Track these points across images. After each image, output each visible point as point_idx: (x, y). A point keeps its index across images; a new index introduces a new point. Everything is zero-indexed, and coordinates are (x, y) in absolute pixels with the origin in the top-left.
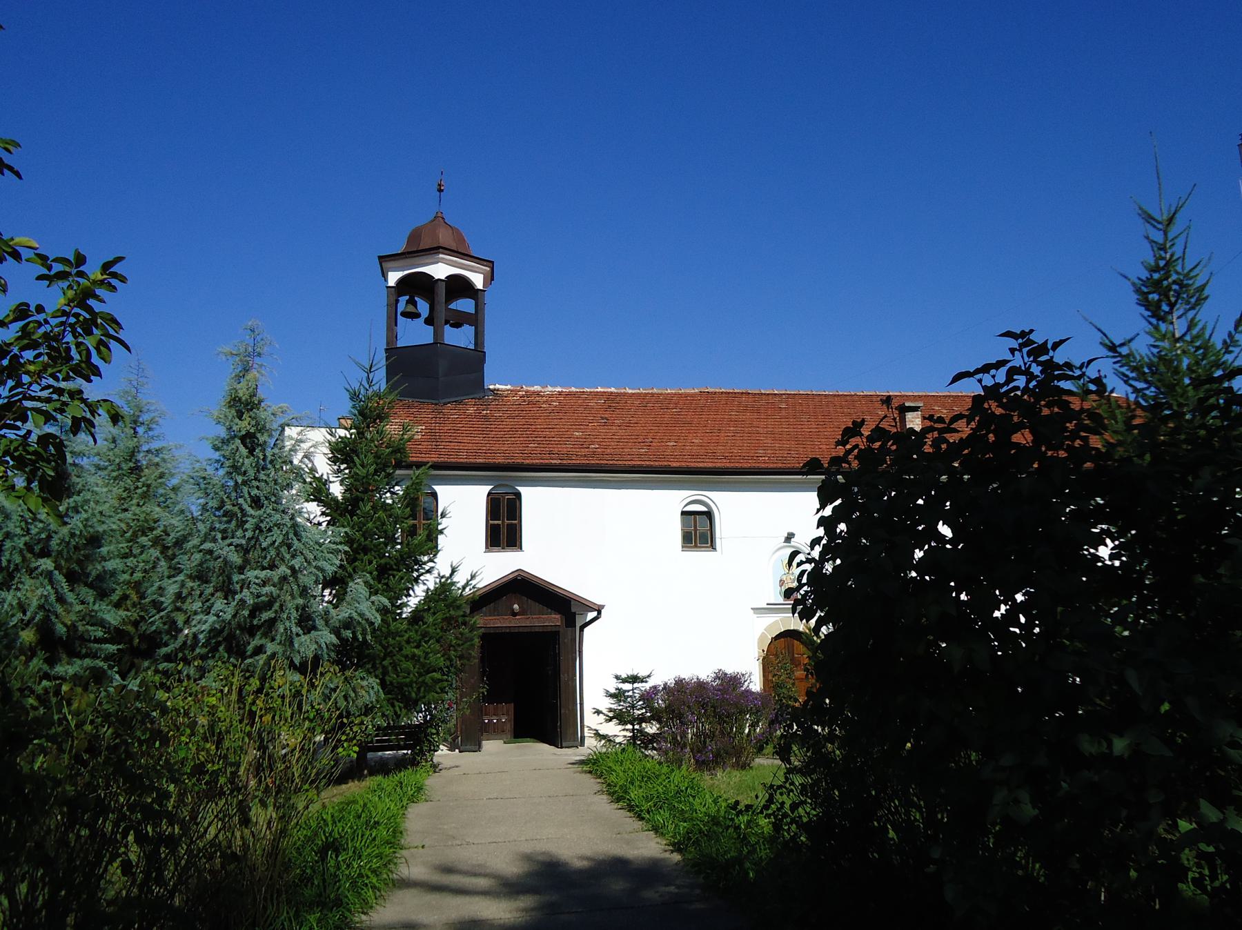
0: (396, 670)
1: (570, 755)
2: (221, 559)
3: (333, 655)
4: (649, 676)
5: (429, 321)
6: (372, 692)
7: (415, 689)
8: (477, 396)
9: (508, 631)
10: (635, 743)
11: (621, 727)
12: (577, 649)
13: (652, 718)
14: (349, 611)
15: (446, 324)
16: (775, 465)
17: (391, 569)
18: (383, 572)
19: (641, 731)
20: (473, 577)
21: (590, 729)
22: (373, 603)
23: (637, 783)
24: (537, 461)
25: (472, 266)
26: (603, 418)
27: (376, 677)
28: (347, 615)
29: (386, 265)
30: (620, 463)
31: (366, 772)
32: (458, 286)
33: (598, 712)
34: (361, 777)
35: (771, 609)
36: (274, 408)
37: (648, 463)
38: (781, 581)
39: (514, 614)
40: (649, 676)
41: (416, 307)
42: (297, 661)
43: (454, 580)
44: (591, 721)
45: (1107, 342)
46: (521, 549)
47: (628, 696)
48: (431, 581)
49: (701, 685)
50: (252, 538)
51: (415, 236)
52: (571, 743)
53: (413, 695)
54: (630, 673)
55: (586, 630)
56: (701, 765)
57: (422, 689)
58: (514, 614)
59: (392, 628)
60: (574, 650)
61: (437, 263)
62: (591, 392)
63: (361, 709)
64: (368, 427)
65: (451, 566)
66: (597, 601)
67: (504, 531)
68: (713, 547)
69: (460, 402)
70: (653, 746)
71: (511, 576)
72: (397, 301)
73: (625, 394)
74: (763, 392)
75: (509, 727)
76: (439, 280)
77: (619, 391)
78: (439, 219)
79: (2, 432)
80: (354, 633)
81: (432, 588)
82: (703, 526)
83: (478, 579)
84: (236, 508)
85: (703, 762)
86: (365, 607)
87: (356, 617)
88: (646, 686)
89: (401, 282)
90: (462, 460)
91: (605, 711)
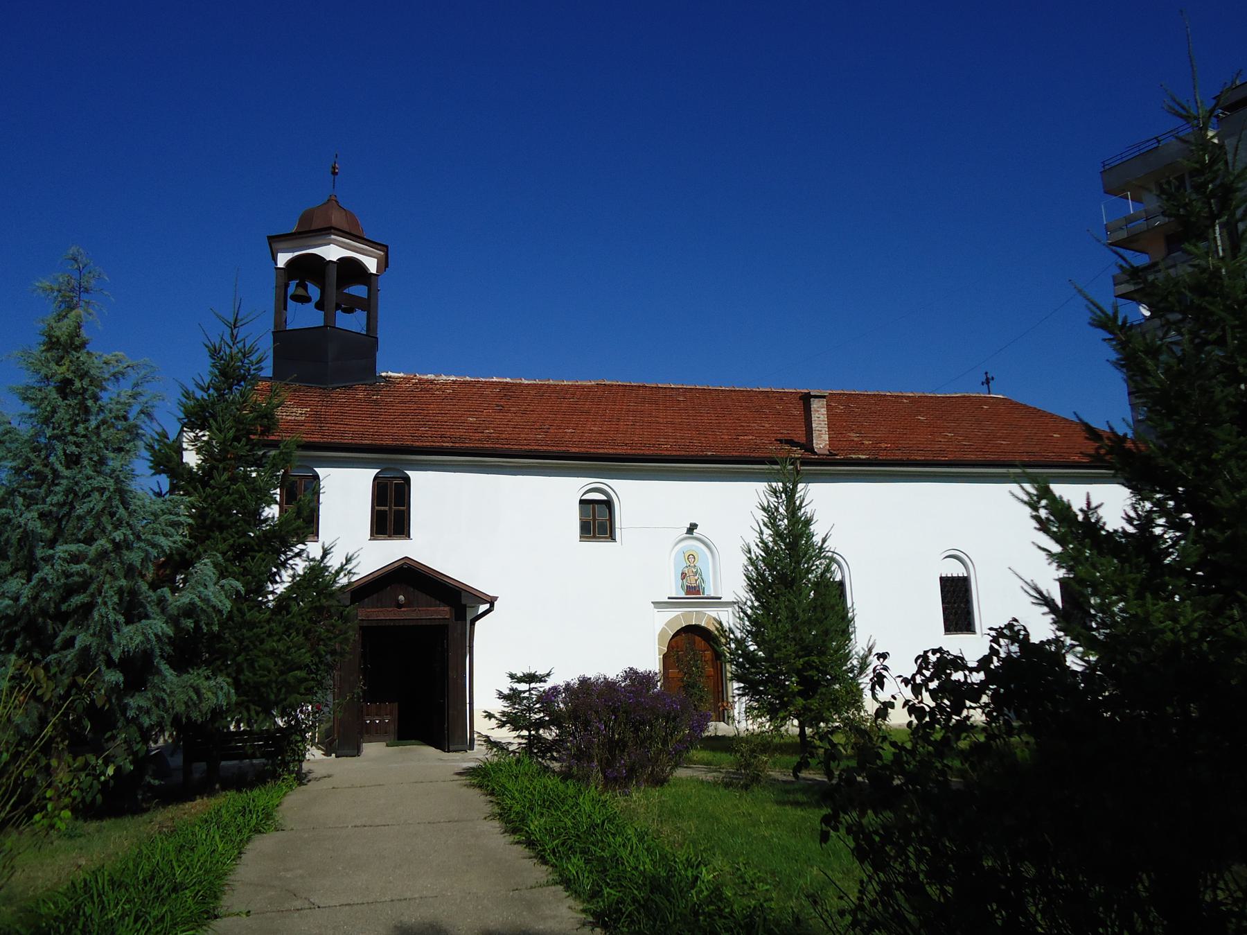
0: (253, 667)
1: (458, 761)
2: (21, 530)
3: (168, 649)
4: (548, 675)
5: (320, 306)
6: (220, 694)
7: (275, 690)
8: (369, 382)
9: (401, 624)
10: (531, 752)
11: (515, 734)
12: (468, 645)
13: (551, 722)
14: (191, 596)
15: (337, 309)
16: (678, 453)
17: (252, 550)
18: (241, 552)
19: (539, 738)
20: (348, 560)
21: (480, 735)
22: (222, 587)
23: (537, 809)
24: (428, 444)
25: (366, 250)
26: (498, 406)
27: (228, 675)
28: (187, 601)
29: (275, 246)
30: (516, 447)
31: (217, 786)
32: (348, 268)
33: (489, 716)
34: (211, 793)
35: (672, 603)
36: (106, 357)
37: (545, 448)
38: (682, 574)
39: (400, 606)
40: (548, 675)
41: (306, 291)
42: (116, 656)
43: (328, 564)
44: (482, 726)
45: (1125, 265)
46: (409, 537)
47: (524, 698)
48: (300, 566)
49: (609, 685)
50: (64, 503)
51: (307, 217)
52: (460, 747)
53: (272, 697)
54: (527, 671)
55: (478, 623)
56: (611, 781)
57: (284, 690)
58: (400, 606)
59: (248, 616)
60: (465, 645)
61: (329, 244)
62: (486, 382)
63: (206, 713)
64: (230, 388)
65: (323, 547)
66: (491, 592)
67: (391, 518)
68: (612, 538)
69: (350, 388)
70: (552, 755)
71: (396, 565)
72: (287, 286)
73: (521, 384)
74: (660, 386)
75: (393, 728)
76: (330, 261)
77: (514, 382)
78: (332, 202)
79: (2, 463)
80: (197, 623)
81: (301, 573)
82: (602, 517)
83: (354, 563)
84: (48, 469)
85: (615, 779)
86: (212, 592)
87: (199, 603)
88: (546, 686)
89: (290, 263)
90: (346, 441)
91: (497, 715)
